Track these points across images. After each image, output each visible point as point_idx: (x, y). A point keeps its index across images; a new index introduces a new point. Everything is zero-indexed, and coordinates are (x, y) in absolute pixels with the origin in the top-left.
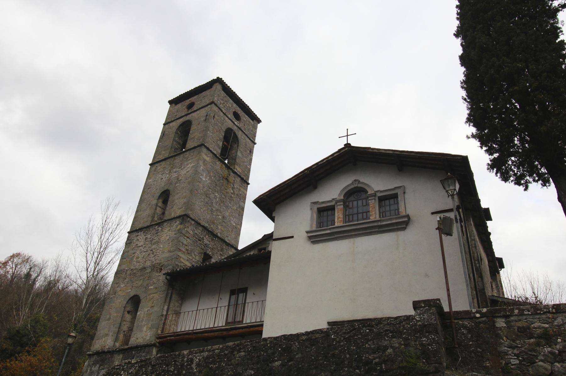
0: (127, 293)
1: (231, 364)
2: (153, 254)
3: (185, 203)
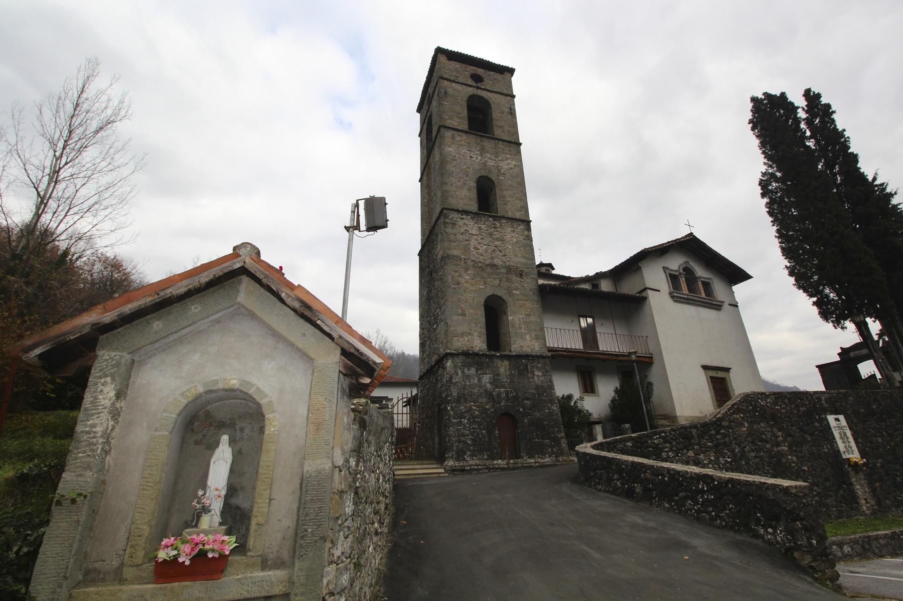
2: (500, 251)
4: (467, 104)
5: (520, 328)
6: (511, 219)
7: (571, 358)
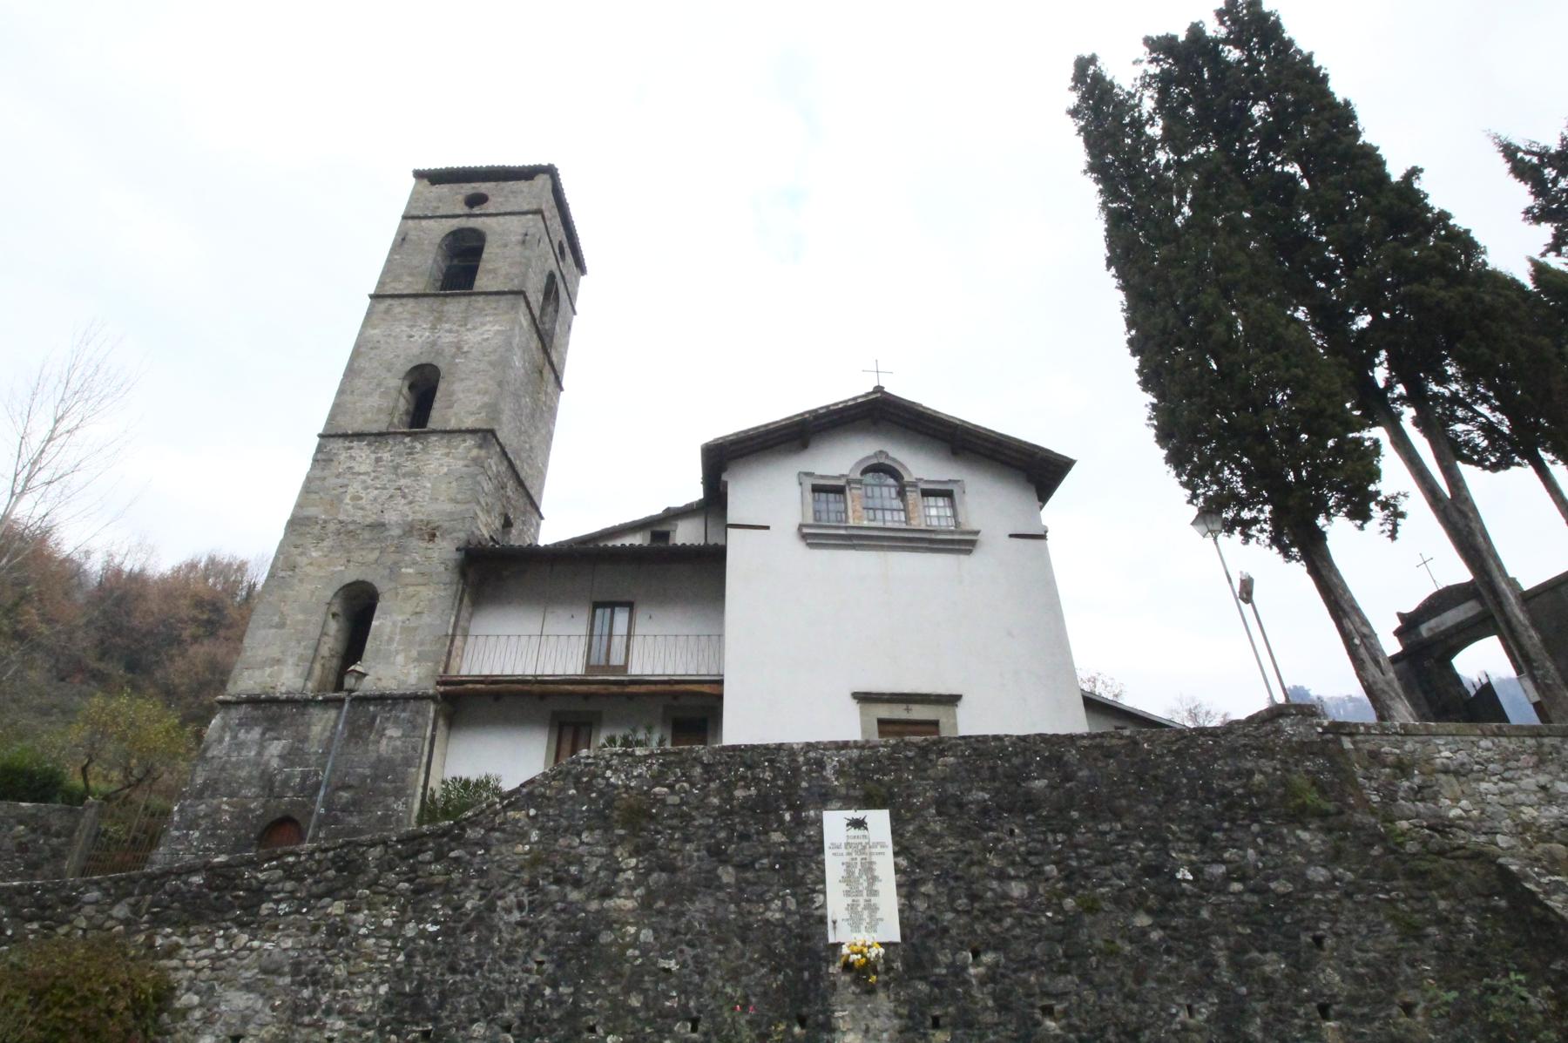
0: (333, 573)
1: (929, 778)
2: (404, 497)
3: (484, 406)
4: (487, 251)
5: (390, 640)
6: (446, 432)
7: (543, 696)
